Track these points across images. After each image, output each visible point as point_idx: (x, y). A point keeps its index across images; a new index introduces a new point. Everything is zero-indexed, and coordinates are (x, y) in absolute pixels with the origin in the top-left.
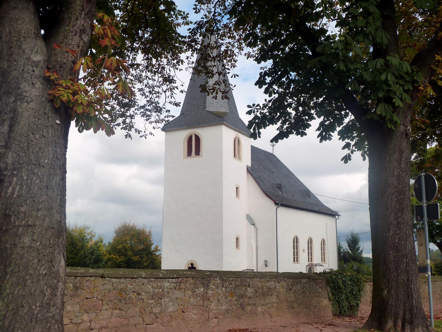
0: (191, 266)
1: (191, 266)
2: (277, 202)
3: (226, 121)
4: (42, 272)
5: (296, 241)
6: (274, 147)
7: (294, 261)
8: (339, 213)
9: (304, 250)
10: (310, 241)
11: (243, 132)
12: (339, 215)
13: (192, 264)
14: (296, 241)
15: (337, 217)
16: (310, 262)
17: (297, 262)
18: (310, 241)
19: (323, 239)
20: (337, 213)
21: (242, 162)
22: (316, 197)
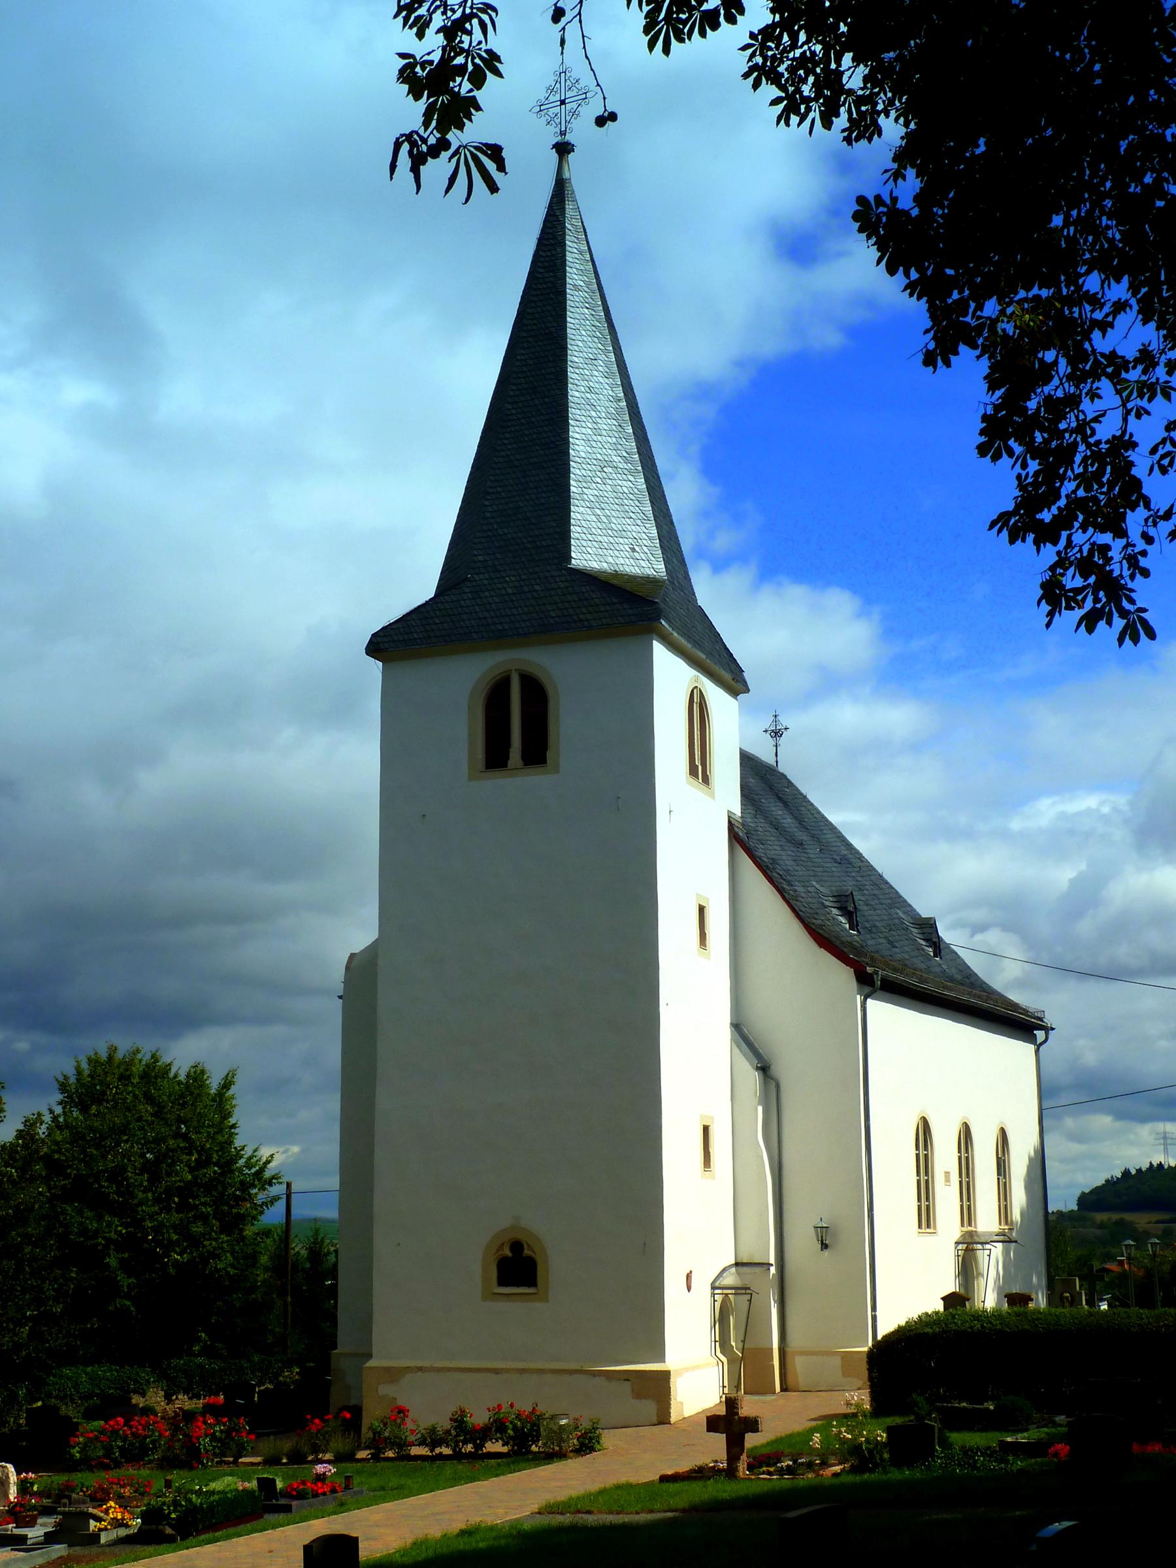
0: (510, 1255)
1: (510, 1255)
2: (869, 970)
3: (668, 621)
4: (1061, 1426)
5: (924, 1133)
6: (782, 741)
7: (920, 1226)
8: (1049, 1020)
9: (947, 1174)
10: (966, 1137)
11: (717, 669)
12: (1047, 1029)
13: (517, 1246)
14: (924, 1133)
15: (1040, 1035)
16: (967, 1229)
17: (928, 1226)
18: (966, 1137)
19: (1002, 1128)
20: (1041, 1019)
21: (713, 796)
22: (956, 953)
